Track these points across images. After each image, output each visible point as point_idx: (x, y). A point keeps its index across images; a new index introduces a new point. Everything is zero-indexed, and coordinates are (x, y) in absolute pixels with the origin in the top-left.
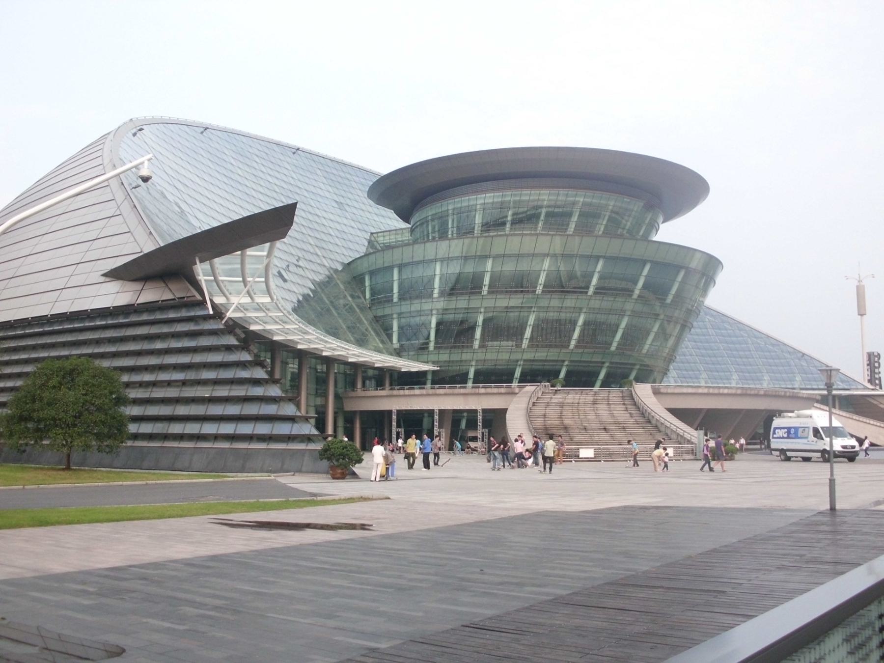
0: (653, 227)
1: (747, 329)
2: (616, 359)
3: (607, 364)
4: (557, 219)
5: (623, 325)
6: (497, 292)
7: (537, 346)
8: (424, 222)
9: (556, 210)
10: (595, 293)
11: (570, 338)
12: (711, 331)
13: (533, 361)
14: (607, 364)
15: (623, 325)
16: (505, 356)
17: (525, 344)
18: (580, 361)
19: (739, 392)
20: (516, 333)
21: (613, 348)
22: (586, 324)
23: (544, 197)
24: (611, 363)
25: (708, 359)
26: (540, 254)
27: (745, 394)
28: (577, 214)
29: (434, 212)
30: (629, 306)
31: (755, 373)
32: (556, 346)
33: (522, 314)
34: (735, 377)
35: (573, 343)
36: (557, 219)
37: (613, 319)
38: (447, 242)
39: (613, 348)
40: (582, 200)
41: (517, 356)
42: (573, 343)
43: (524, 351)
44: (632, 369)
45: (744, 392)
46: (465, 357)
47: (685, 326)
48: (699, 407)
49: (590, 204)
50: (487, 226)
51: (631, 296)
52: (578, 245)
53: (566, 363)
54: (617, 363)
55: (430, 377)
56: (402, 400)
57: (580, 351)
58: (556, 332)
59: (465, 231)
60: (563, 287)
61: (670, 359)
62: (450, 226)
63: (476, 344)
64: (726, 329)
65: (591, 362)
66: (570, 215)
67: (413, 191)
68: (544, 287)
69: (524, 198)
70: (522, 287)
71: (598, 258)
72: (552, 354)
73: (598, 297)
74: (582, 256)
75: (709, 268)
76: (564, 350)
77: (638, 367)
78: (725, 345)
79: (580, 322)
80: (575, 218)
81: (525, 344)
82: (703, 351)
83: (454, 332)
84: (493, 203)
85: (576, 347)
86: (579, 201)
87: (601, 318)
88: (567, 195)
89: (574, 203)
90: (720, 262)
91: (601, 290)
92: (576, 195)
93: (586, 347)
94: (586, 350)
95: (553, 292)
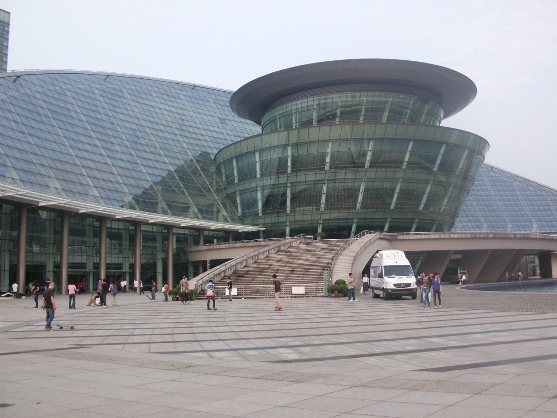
0: (434, 116)
1: (546, 189)
2: (396, 216)
3: (417, 221)
4: (350, 115)
5: (427, 191)
6: (306, 170)
7: (331, 209)
8: (273, 120)
9: (346, 109)
10: (370, 166)
11: (420, 201)
12: (518, 193)
13: (338, 219)
14: (417, 221)
15: (427, 191)
16: (308, 217)
17: (322, 207)
18: (365, 219)
19: (468, 236)
20: (314, 200)
21: (392, 206)
22: (366, 190)
23: (338, 99)
24: (392, 219)
25: (539, 213)
26: (332, 140)
27: (496, 238)
28: (388, 110)
29: (281, 112)
30: (400, 175)
31: (551, 222)
32: (345, 208)
33: (346, 184)
34: (535, 226)
35: (359, 205)
36: (350, 115)
37: (387, 185)
38: (277, 134)
39: (392, 206)
40: (391, 100)
41: (318, 217)
42: (359, 205)
43: (321, 213)
44: (413, 223)
45: (474, 236)
46: (282, 219)
47: (463, 189)
48: (447, 249)
49: (373, 102)
50: (321, 121)
51: (400, 168)
52: (391, 131)
53: (389, 220)
54: (396, 218)
55: (261, 235)
56: (217, 252)
57: (365, 211)
58: (352, 197)
59: (288, 127)
60: (354, 163)
61: (454, 216)
62: (294, 122)
63: (288, 209)
64: (530, 191)
65: (374, 219)
66: (359, 112)
67: (261, 99)
68: (408, 164)
69: (335, 100)
70: (354, 163)
71: (409, 141)
72: (343, 214)
73: (373, 169)
74: (355, 140)
75: (477, 145)
76: (351, 211)
77: (389, 220)
78: (528, 202)
79: (398, 190)
80: (386, 114)
81: (322, 207)
82: (511, 208)
83: (274, 203)
84: (307, 106)
85: (362, 208)
86: (388, 101)
87: (377, 185)
88: (320, 100)
89: (385, 102)
90: (482, 139)
91: (373, 164)
92: (387, 97)
93: (368, 208)
94: (369, 210)
95: (347, 167)
